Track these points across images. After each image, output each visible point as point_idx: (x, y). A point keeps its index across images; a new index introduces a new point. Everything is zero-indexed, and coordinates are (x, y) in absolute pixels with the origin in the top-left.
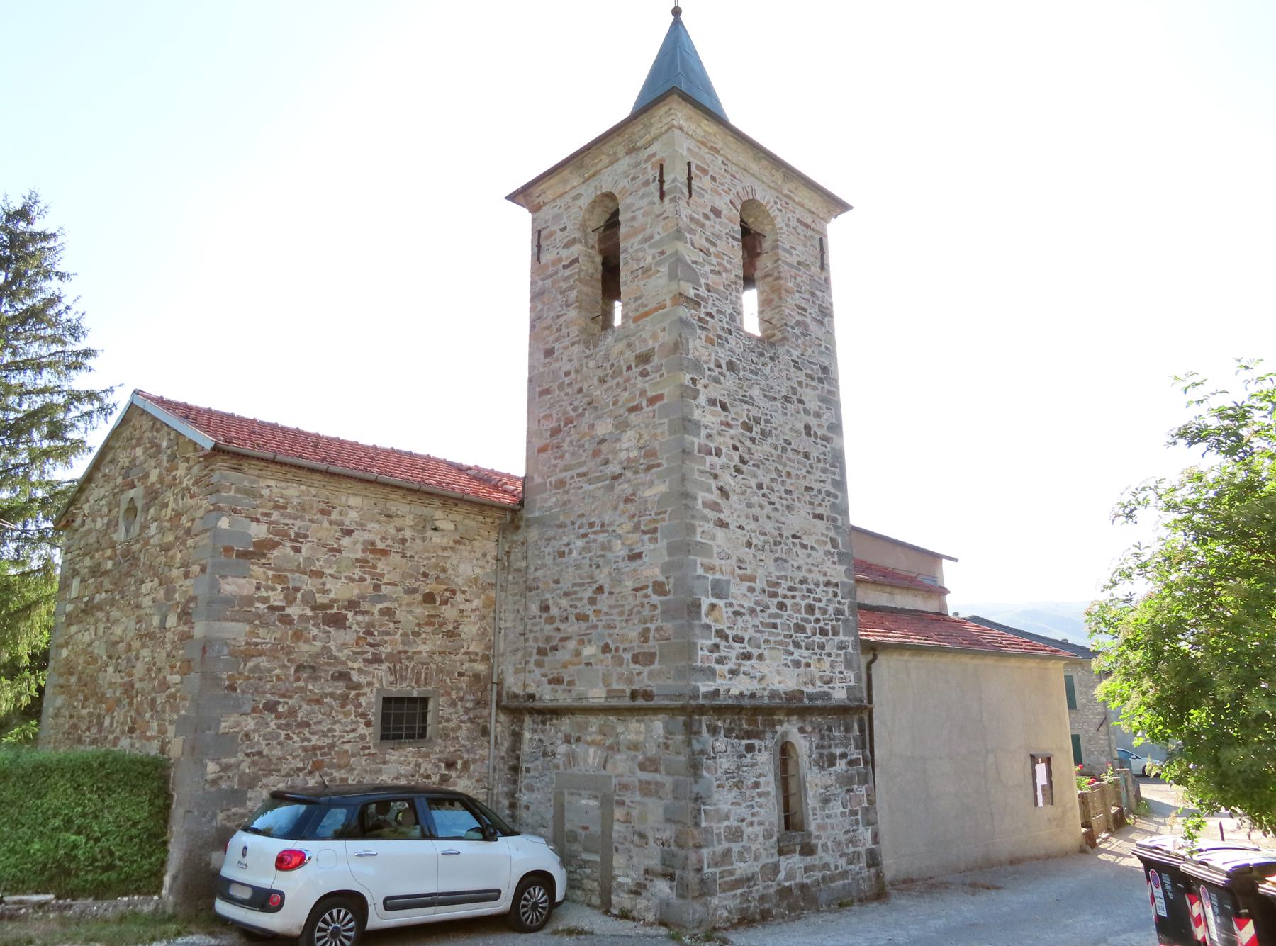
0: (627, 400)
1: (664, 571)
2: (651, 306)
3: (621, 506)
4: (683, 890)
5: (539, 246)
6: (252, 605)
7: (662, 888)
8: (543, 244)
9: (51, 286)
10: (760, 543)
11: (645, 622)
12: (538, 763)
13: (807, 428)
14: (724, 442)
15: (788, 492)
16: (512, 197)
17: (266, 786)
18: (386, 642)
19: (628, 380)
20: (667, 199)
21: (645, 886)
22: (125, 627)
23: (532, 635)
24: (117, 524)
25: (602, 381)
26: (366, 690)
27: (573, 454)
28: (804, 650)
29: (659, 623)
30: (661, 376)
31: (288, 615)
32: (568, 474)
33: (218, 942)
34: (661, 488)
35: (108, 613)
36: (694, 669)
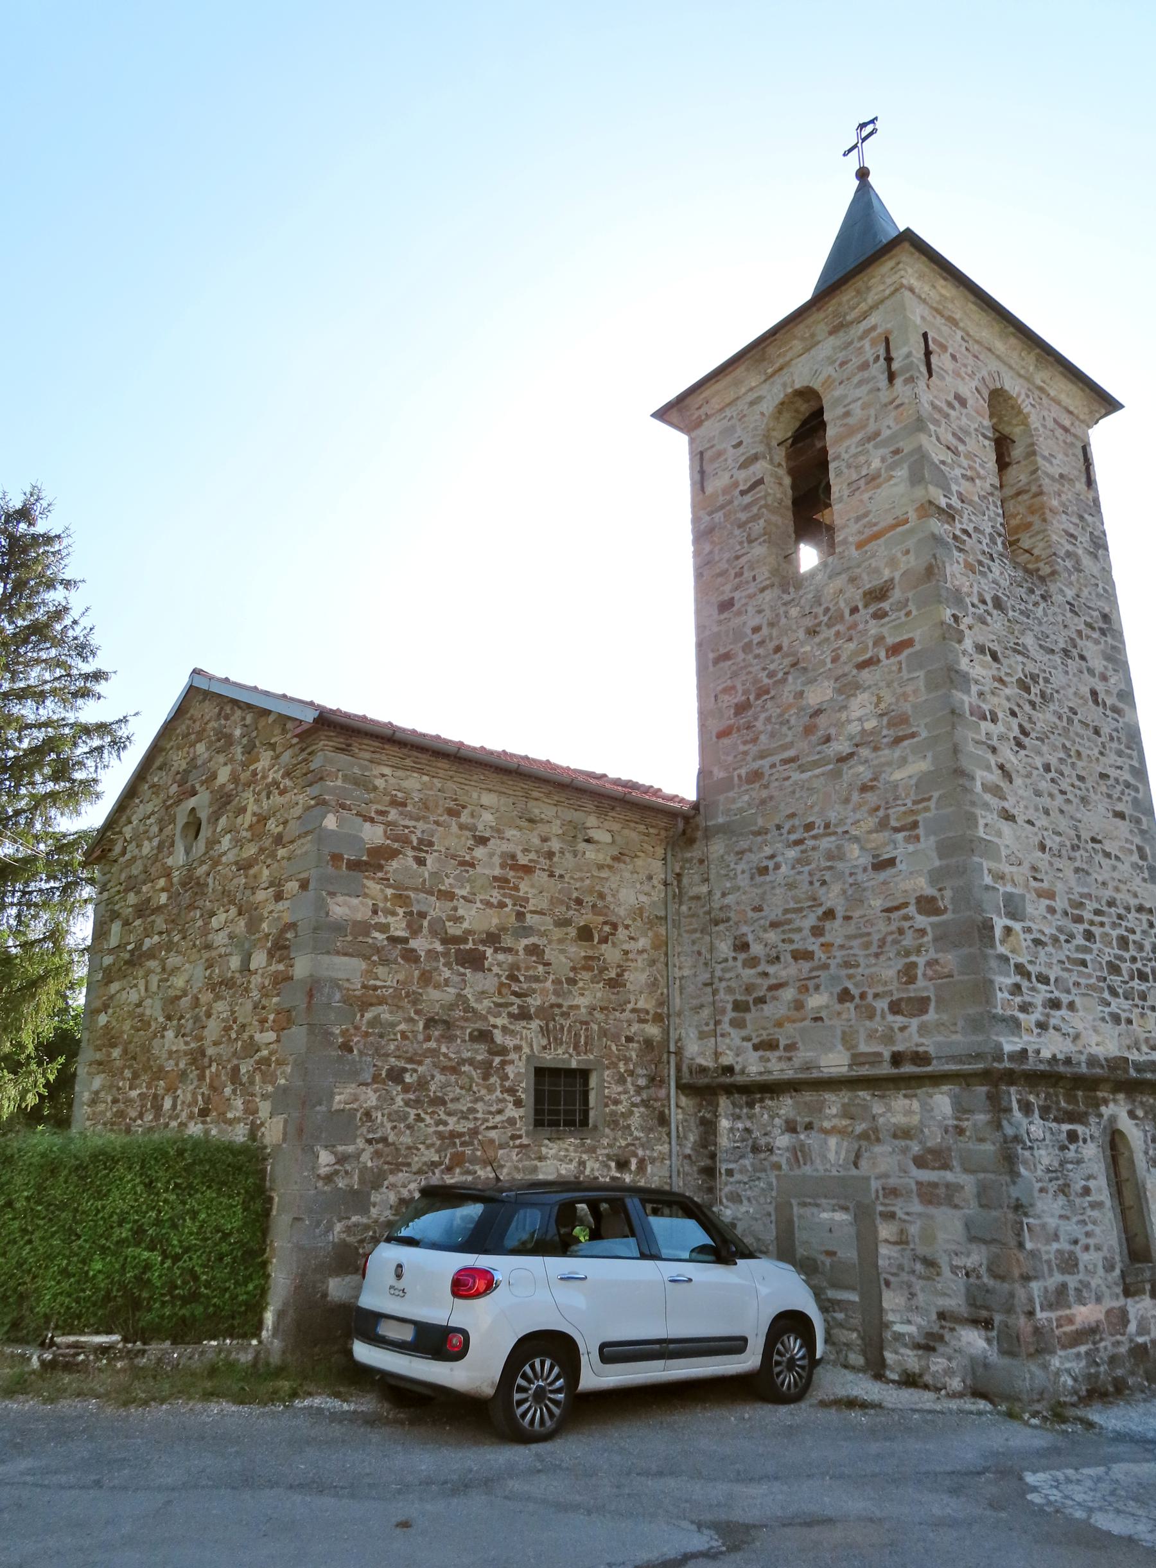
0: (855, 653)
1: (933, 881)
2: (882, 525)
3: (855, 797)
4: (1009, 1344)
5: (702, 472)
6: (367, 934)
7: (973, 1340)
8: (709, 469)
9: (56, 596)
10: (1055, 847)
11: (908, 954)
12: (746, 1162)
13: (1094, 693)
14: (998, 704)
15: (1081, 778)
16: (662, 414)
17: (392, 1186)
18: (534, 991)
19: (854, 626)
20: (899, 381)
21: (941, 1338)
22: (189, 974)
23: (724, 984)
24: (172, 845)
25: (812, 632)
26: (513, 1056)
27: (772, 735)
28: (1122, 1000)
29: (932, 955)
30: (908, 614)
31: (413, 950)
32: (766, 763)
33: (345, 1407)
34: (920, 766)
35: (163, 962)
36: (994, 1016)
